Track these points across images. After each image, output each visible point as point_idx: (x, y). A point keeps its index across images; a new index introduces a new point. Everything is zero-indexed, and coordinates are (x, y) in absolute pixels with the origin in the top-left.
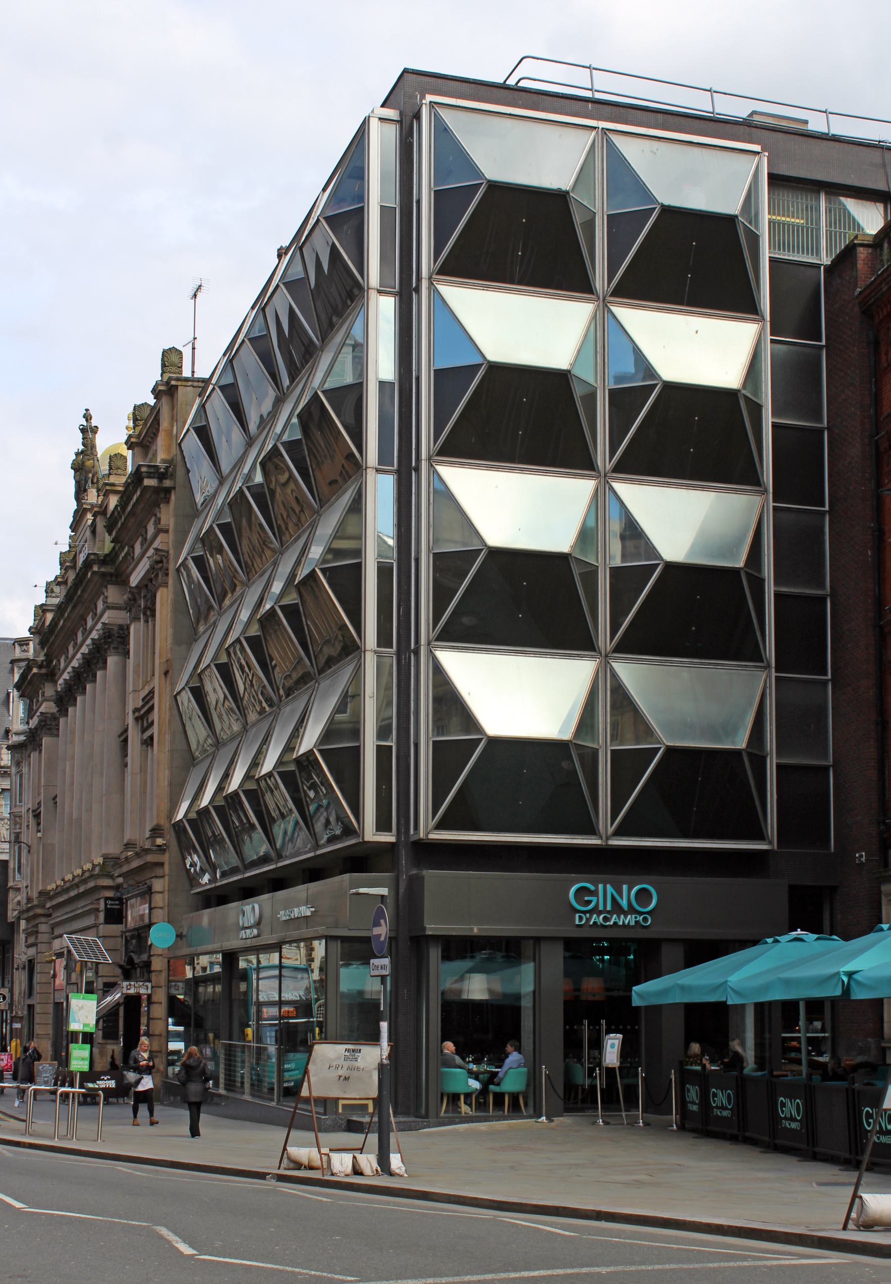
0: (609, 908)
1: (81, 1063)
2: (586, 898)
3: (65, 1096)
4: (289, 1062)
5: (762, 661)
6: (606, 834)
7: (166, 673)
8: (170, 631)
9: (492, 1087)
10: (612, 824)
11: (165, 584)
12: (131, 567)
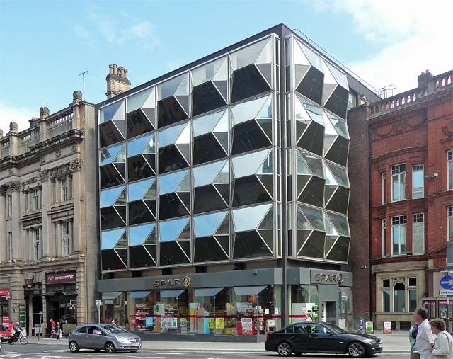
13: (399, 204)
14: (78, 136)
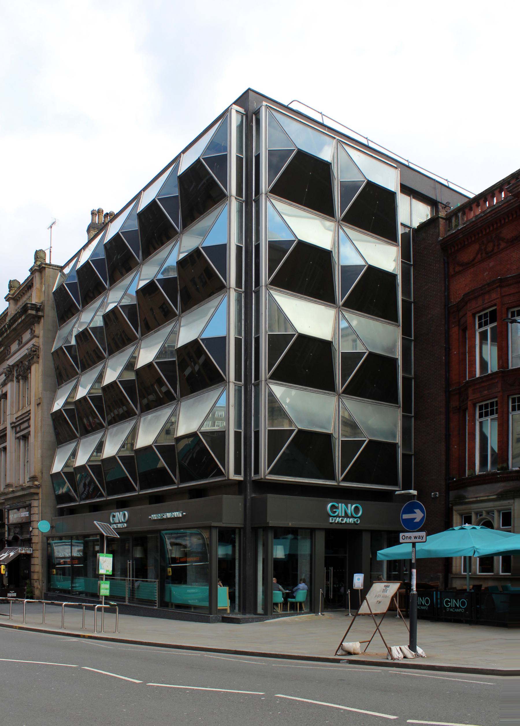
0: (343, 515)
1: (105, 591)
2: (334, 510)
3: (99, 609)
4: (76, 583)
5: (398, 404)
6: (339, 480)
7: (38, 405)
8: (41, 384)
9: (290, 600)
10: (341, 476)
11: (38, 362)
12: (8, 357)
13: (488, 379)
14: (34, 312)
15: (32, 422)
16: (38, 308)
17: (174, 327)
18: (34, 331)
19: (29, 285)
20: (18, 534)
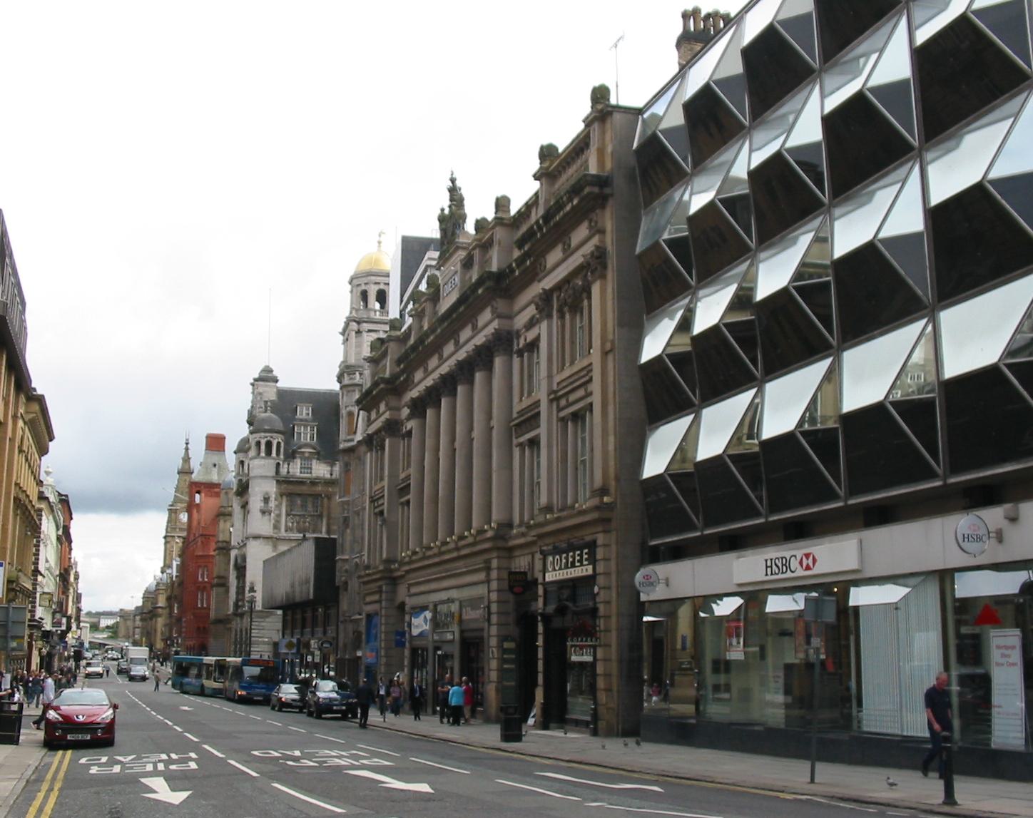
12: (412, 386)
15: (596, 387)
16: (602, 181)
17: (691, 302)
18: (596, 222)
19: (580, 146)
20: (567, 600)
